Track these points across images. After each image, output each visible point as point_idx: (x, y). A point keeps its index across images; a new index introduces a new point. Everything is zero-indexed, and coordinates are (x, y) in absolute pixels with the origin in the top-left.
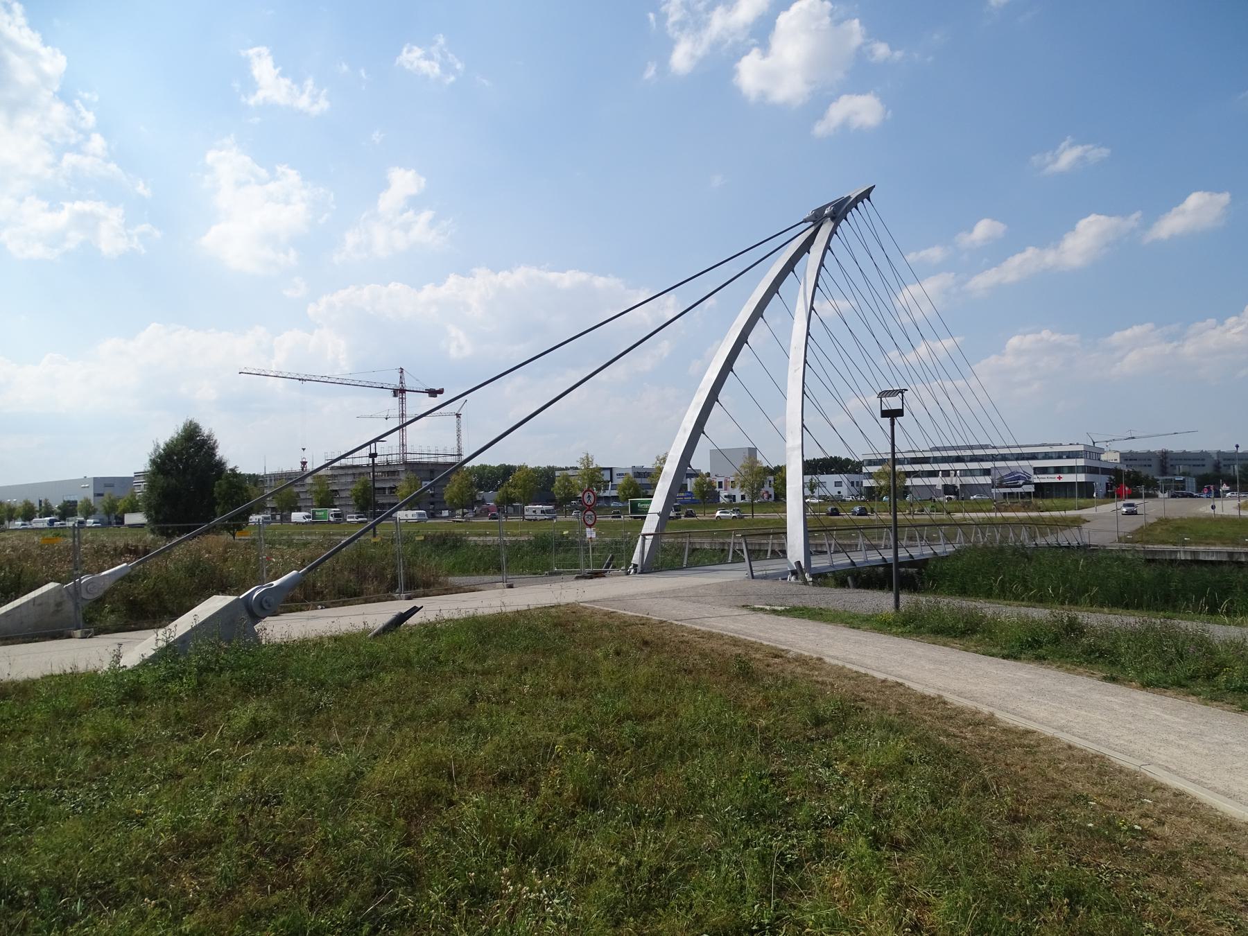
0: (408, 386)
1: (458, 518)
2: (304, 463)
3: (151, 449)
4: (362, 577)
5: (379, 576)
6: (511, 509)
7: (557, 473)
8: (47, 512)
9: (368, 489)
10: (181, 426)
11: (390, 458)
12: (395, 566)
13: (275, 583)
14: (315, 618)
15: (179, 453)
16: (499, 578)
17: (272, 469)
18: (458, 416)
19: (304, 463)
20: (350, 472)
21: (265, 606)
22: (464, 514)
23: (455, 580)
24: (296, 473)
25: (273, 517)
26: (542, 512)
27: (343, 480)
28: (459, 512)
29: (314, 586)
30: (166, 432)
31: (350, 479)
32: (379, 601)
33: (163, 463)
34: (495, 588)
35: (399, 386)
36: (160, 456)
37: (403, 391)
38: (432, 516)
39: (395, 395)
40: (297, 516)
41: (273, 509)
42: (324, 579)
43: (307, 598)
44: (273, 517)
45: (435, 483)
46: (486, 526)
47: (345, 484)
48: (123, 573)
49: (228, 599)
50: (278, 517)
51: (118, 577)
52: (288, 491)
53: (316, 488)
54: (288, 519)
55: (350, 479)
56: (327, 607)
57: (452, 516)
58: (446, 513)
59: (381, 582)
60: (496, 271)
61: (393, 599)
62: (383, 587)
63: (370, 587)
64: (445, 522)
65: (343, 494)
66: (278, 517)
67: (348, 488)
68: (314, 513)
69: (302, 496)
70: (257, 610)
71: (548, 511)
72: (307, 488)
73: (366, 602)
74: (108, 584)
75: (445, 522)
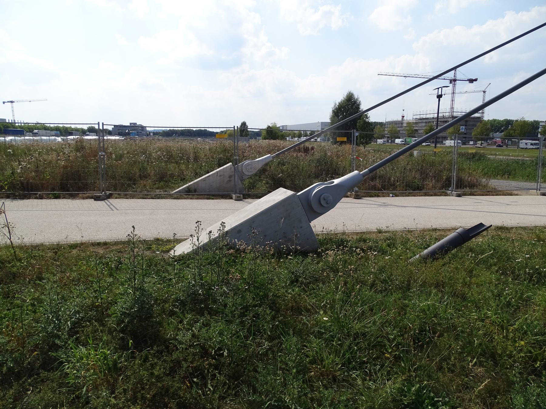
0: (458, 77)
1: (479, 146)
2: (403, 117)
3: (333, 106)
4: (424, 175)
5: (437, 176)
6: (510, 142)
7: (541, 124)
8: (306, 135)
9: (434, 130)
10: (346, 94)
11: (445, 114)
12: (450, 170)
13: (336, 181)
14: (385, 205)
15: (344, 107)
16: (533, 185)
17: (389, 119)
18: (484, 92)
19: (403, 117)
20: (424, 121)
21: (323, 202)
22: (482, 143)
23: (494, 183)
24: (399, 121)
25: (388, 141)
26: (532, 144)
27: (420, 125)
28: (480, 142)
29: (390, 179)
30: (339, 97)
31: (424, 124)
32: (435, 195)
33: (337, 112)
34: (527, 194)
35: (453, 78)
36: (336, 109)
37: (455, 80)
38: (464, 144)
39: (451, 83)
40: (398, 141)
41: (388, 137)
42: (398, 175)
43: (384, 188)
44: (388, 141)
45: (469, 125)
46: (494, 150)
47: (421, 127)
48: (267, 161)
49: (289, 193)
50: (390, 141)
51: (264, 163)
52: (394, 129)
53: (408, 128)
54: (394, 142)
55: (424, 124)
56: (396, 196)
57: (474, 144)
58: (471, 143)
59: (438, 181)
60: (517, 12)
61: (446, 195)
62: (439, 185)
63: (430, 183)
64: (471, 148)
65: (420, 132)
66: (390, 141)
67: (422, 128)
68: (405, 139)
69: (401, 132)
70: (315, 206)
71: (535, 144)
72: (404, 128)
73: (426, 195)
74: (259, 167)
75: (471, 148)
